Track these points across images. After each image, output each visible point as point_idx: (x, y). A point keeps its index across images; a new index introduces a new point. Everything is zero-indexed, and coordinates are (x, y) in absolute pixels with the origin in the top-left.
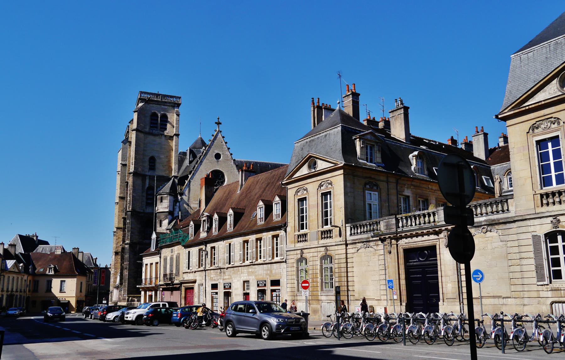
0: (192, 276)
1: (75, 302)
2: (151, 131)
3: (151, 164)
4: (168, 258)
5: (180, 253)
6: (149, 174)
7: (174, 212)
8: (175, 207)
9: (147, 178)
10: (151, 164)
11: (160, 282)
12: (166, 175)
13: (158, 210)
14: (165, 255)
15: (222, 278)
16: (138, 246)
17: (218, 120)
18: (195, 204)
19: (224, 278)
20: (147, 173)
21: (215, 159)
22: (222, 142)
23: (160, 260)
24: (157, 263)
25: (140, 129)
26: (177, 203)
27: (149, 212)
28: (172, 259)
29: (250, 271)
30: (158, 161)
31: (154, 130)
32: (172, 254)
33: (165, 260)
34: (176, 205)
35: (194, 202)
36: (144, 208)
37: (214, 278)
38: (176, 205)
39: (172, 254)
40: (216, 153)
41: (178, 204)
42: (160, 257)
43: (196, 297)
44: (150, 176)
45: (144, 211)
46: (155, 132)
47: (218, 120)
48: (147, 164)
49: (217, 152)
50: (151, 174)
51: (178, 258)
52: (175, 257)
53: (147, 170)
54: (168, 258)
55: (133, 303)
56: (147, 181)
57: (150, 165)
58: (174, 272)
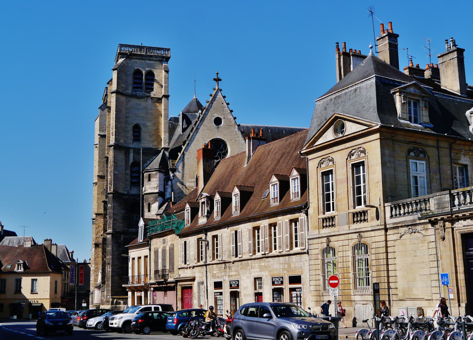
2: (134, 92)
4: (160, 251)
6: (133, 147)
7: (166, 193)
8: (167, 187)
12: (154, 147)
15: (228, 274)
17: (217, 76)
19: (230, 275)
20: (131, 146)
22: (223, 104)
23: (150, 252)
24: (146, 257)
25: (121, 91)
26: (168, 182)
28: (164, 251)
30: (143, 129)
31: (138, 91)
32: (165, 245)
33: (156, 252)
35: (190, 180)
36: (129, 188)
37: (217, 275)
38: (167, 185)
39: (165, 245)
41: (170, 183)
42: (150, 250)
46: (139, 94)
47: (217, 76)
48: (130, 134)
49: (216, 115)
50: (136, 147)
51: (172, 249)
52: (168, 249)
53: (131, 141)
54: (160, 251)
55: (118, 306)
56: (131, 155)
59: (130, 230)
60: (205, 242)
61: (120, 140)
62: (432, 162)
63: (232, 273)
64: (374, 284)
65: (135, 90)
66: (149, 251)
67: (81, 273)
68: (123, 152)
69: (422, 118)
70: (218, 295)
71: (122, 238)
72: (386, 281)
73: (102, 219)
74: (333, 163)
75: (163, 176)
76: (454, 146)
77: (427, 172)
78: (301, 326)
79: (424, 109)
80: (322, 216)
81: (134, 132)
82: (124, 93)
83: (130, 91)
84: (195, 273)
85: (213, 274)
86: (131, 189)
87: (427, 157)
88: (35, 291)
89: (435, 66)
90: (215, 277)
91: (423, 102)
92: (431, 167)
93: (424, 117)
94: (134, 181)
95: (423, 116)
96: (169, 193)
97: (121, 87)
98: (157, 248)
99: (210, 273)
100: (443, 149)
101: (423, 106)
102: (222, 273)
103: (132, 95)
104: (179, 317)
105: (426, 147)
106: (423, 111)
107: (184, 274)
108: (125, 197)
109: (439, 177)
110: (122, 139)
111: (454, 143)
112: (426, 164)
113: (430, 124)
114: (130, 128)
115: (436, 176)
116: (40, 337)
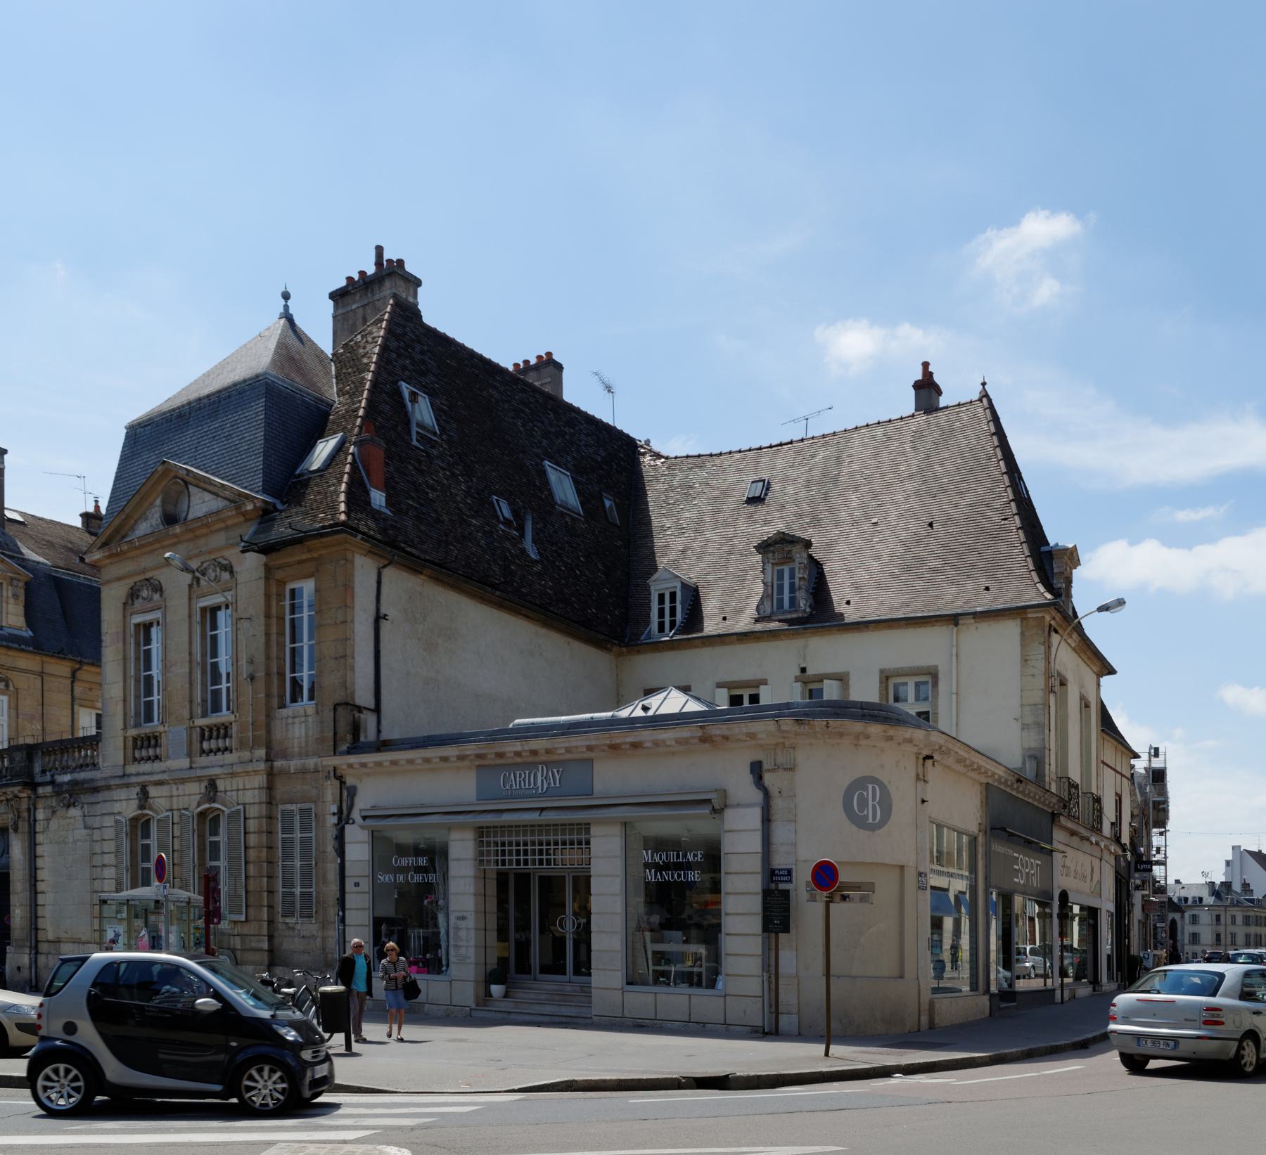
62: (25, 699)
67: (1163, 925)
69: (7, 617)
70: (783, 875)
72: (265, 932)
74: (161, 596)
76: (80, 675)
77: (9, 717)
79: (11, 601)
80: (132, 732)
87: (12, 688)
88: (81, 706)
89: (261, 513)
91: (10, 588)
92: (19, 708)
93: (9, 616)
95: (7, 613)
100: (53, 679)
101: (10, 595)
105: (9, 672)
106: (9, 605)
109: (39, 728)
111: (79, 669)
112: (9, 702)
113: (26, 631)
115: (32, 724)
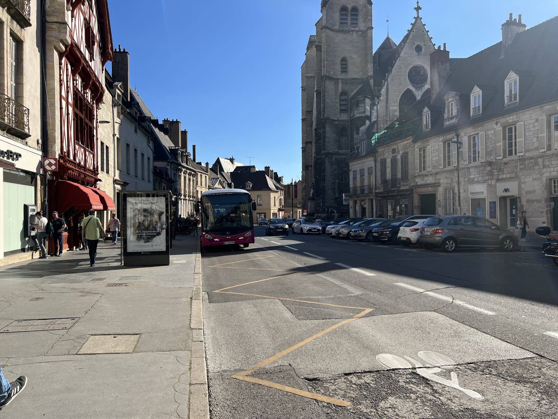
0: (431, 179)
1: (417, 280)
2: (341, 28)
3: (343, 66)
4: (389, 161)
5: (409, 151)
6: (342, 78)
7: (372, 117)
8: (373, 111)
9: (340, 81)
10: (343, 66)
11: (376, 190)
12: (359, 77)
13: (353, 116)
14: (382, 157)
15: (495, 177)
16: (334, 156)
17: (418, 5)
18: (395, 106)
19: (500, 178)
20: (339, 77)
21: (416, 52)
22: (423, 31)
23: (375, 164)
24: (370, 169)
25: (330, 27)
26: (374, 107)
27: (344, 119)
28: (394, 161)
29: (48, 224)
30: (350, 61)
31: (344, 27)
32: (395, 154)
33: (384, 162)
34: (373, 109)
35: (393, 104)
36: (339, 115)
37: (476, 179)
38: (373, 109)
39: (395, 154)
40: (416, 45)
41: (375, 108)
42: (375, 161)
43: (440, 206)
44: (342, 79)
45: (338, 119)
46: (345, 29)
47: (418, 5)
48: (338, 67)
49: (417, 43)
50: (344, 77)
51: (405, 157)
52: (399, 157)
53: (339, 73)
54: (389, 161)
55: (333, 214)
56: (340, 85)
57: (342, 68)
58: (399, 176)
59: (340, 151)
60: (457, 145)
61: (330, 72)
63: (505, 175)
64: (490, 203)
65: (342, 25)
66: (374, 162)
68: (333, 82)
71: (334, 158)
73: (326, 135)
75: (369, 101)
78: (40, 211)
81: (342, 65)
82: (333, 29)
83: (337, 27)
84: (440, 179)
85: (469, 179)
86: (340, 115)
90: (473, 182)
94: (343, 108)
96: (375, 116)
97: (330, 23)
98: (384, 159)
99: (465, 178)
102: (485, 177)
103: (340, 30)
104: (40, 218)
107: (423, 181)
108: (335, 123)
110: (332, 71)
114: (338, 61)
116: (480, 314)
